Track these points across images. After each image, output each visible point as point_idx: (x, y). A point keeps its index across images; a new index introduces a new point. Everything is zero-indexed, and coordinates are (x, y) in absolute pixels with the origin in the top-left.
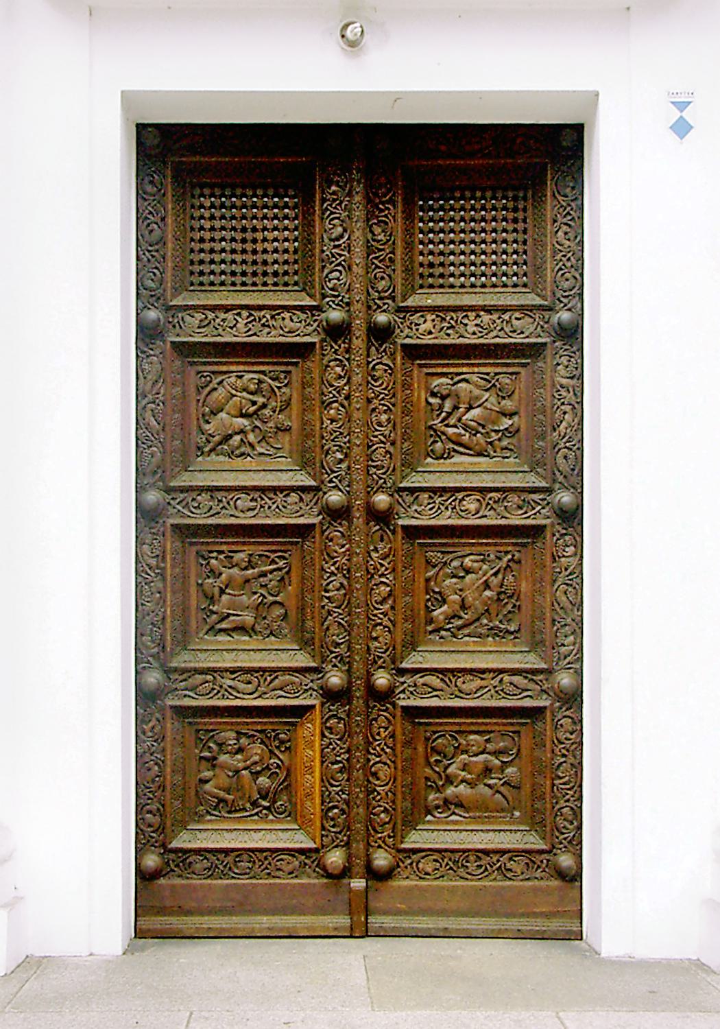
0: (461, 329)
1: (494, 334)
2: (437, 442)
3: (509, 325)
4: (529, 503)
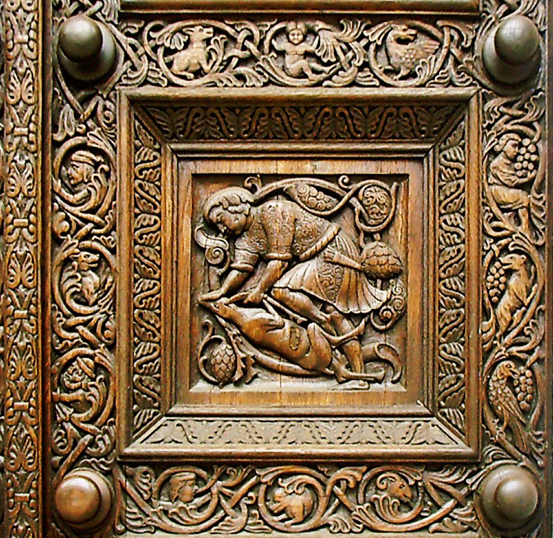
0: (273, 65)
1: (349, 74)
2: (219, 341)
3: (382, 54)
4: (425, 490)
